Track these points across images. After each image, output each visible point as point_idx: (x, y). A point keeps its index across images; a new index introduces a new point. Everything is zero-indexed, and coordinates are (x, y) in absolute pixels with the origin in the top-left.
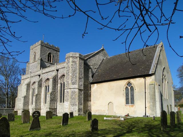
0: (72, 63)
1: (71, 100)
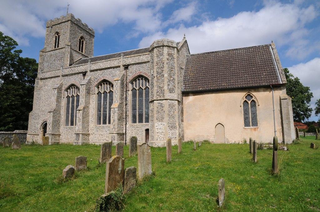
0: (168, 57)
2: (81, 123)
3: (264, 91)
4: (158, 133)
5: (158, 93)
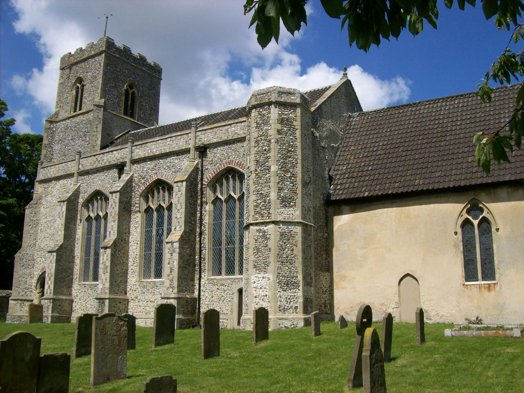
0: (279, 127)
1: (278, 264)
2: (108, 275)
3: (353, 211)
4: (256, 297)
5: (258, 209)
